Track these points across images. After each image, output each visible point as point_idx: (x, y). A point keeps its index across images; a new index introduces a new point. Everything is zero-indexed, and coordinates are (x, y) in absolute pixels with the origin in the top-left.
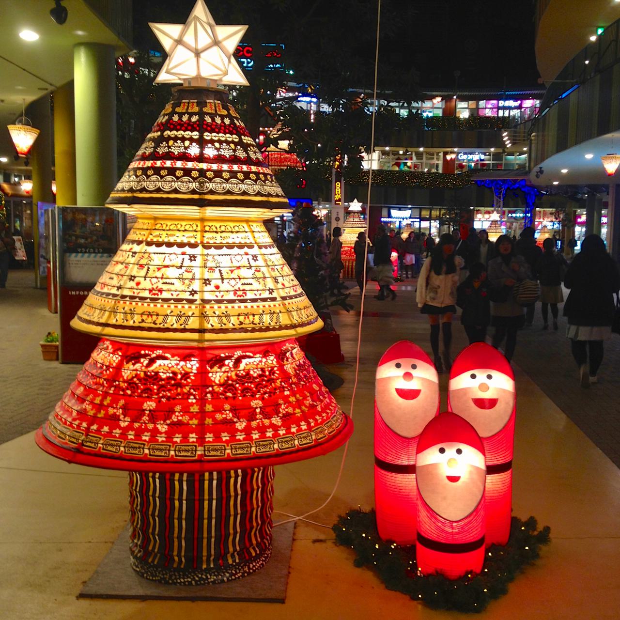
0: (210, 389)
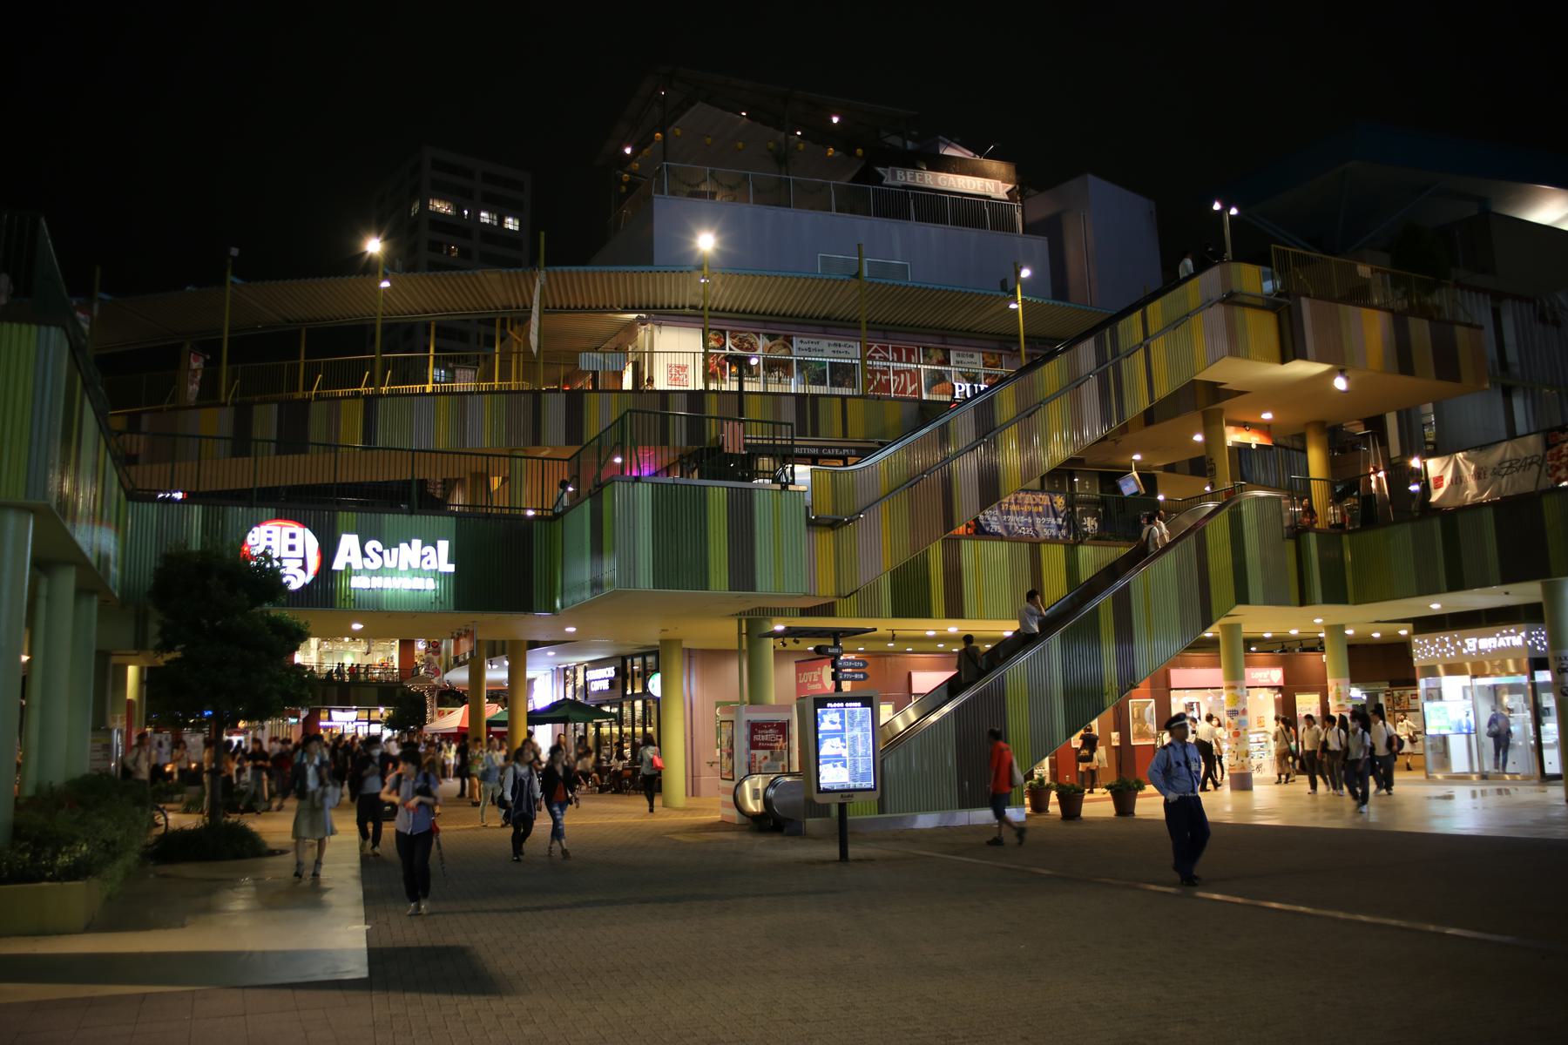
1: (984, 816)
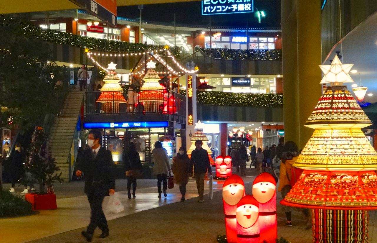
0: (330, 185)
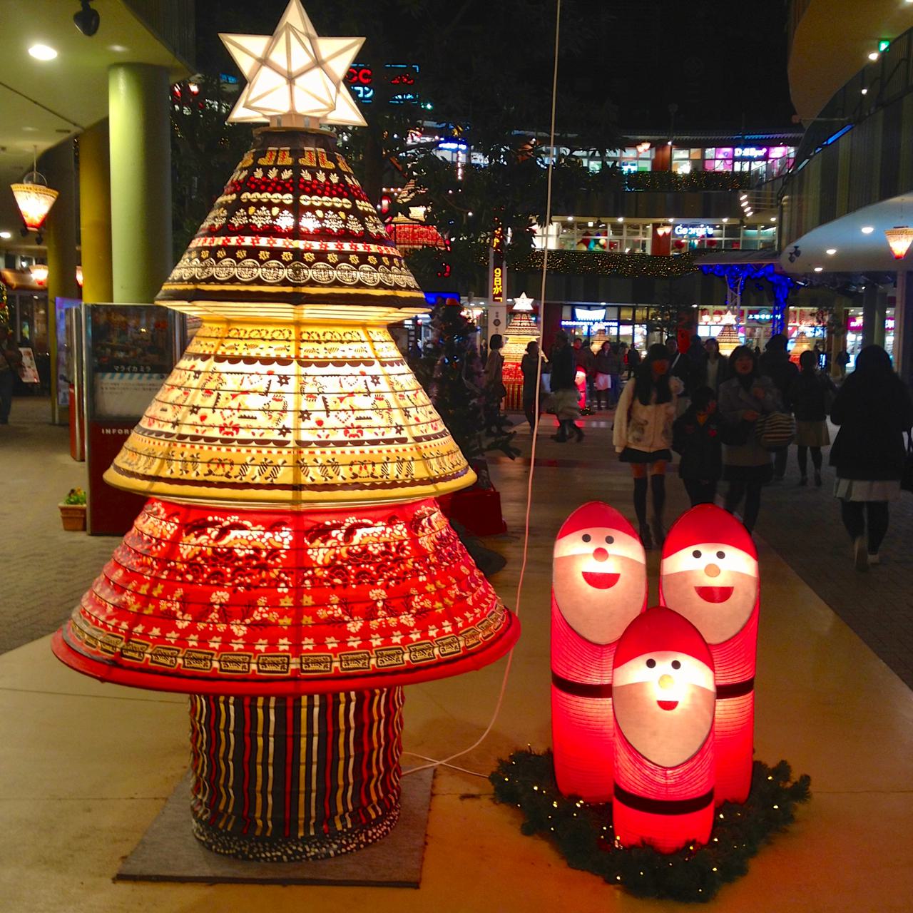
0: (310, 572)
1: (576, 153)
